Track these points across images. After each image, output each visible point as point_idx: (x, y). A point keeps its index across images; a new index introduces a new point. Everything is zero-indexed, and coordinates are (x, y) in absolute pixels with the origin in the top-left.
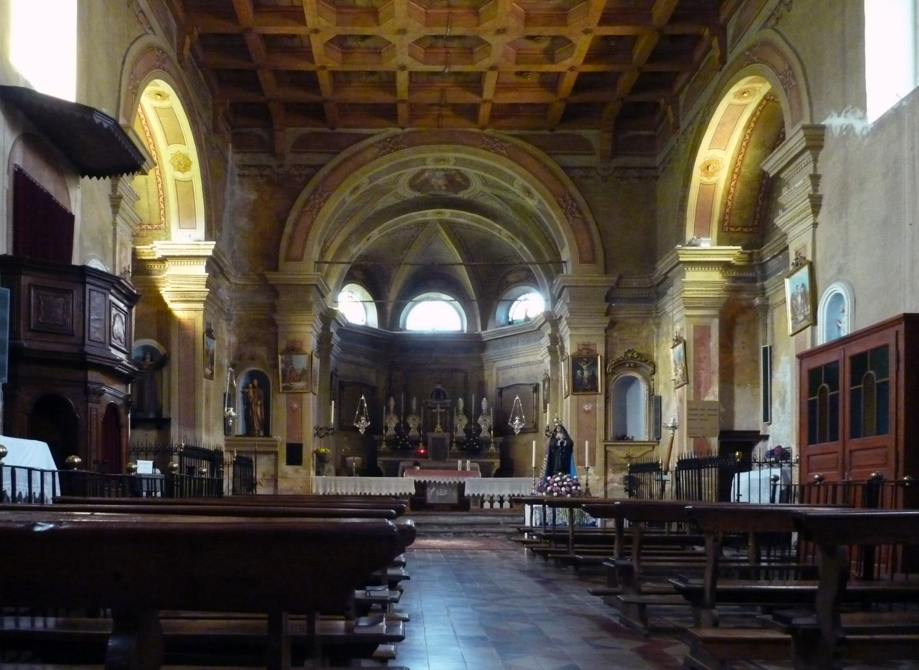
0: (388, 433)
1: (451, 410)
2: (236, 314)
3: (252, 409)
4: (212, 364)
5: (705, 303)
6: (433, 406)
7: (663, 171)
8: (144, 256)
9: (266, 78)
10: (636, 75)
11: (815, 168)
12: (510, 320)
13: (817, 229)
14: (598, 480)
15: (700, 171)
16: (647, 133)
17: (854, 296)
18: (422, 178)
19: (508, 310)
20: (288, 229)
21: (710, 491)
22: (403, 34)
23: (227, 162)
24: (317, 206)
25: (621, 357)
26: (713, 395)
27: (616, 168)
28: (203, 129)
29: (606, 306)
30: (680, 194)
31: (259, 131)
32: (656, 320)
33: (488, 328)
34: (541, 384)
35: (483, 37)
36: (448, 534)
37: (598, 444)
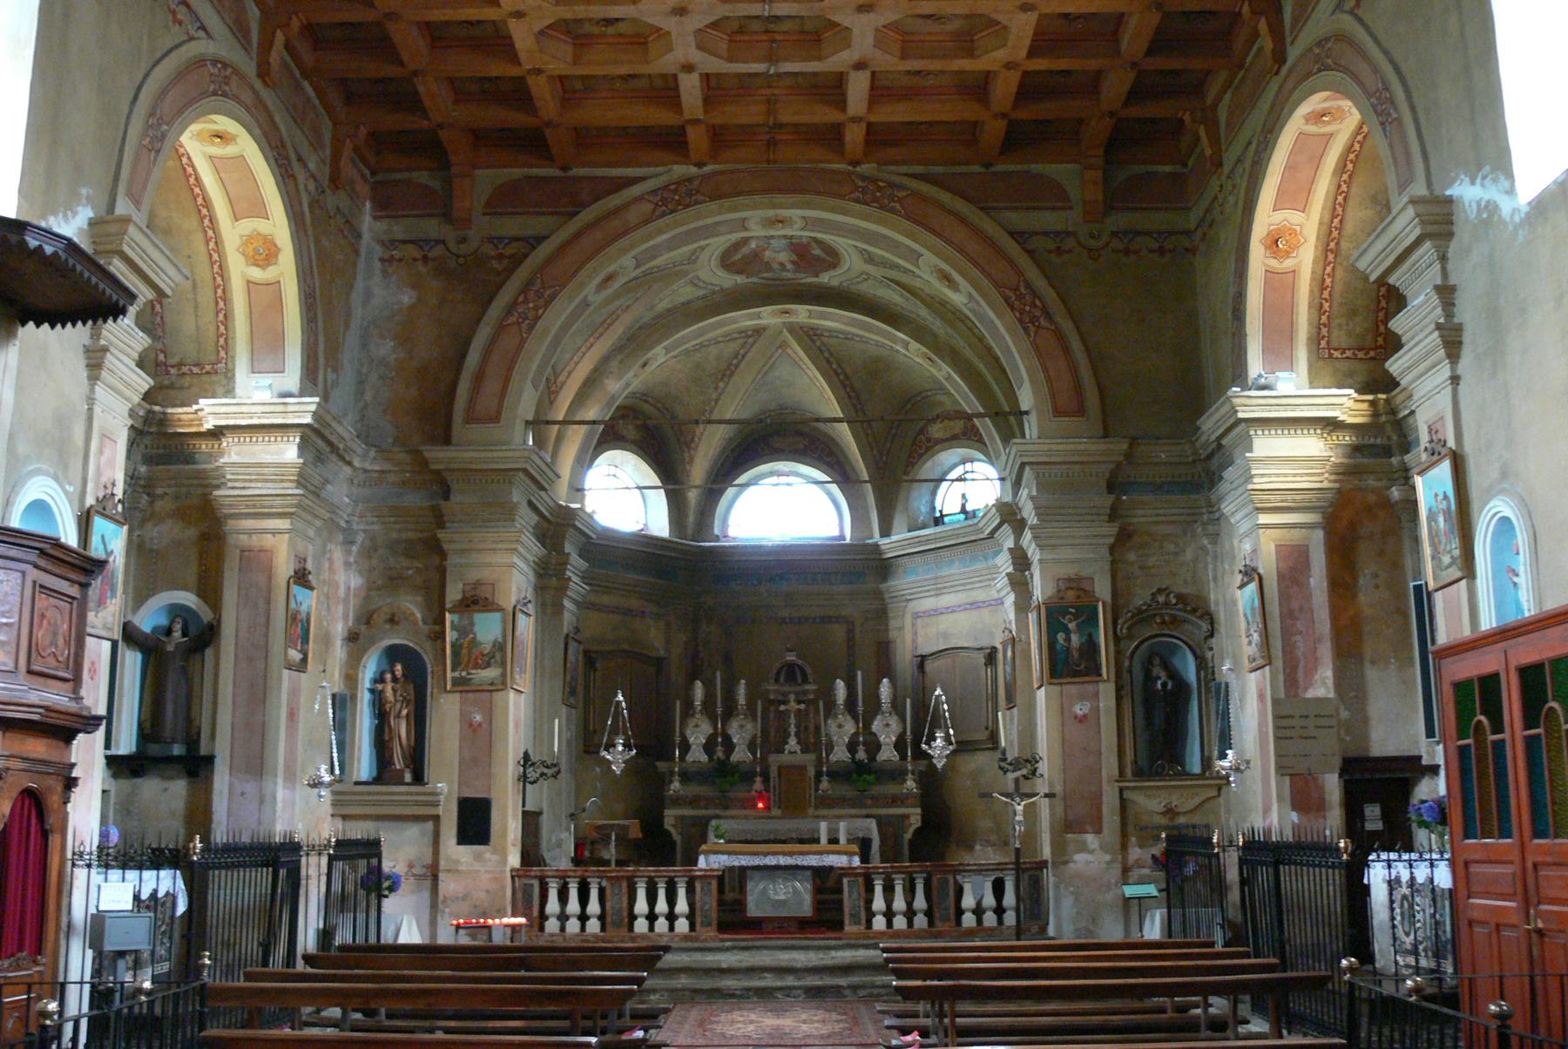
2: (365, 531)
3: (390, 726)
4: (306, 640)
5: (1294, 501)
6: (780, 698)
7: (1203, 239)
8: (182, 426)
9: (433, 92)
10: (1132, 76)
11: (1445, 273)
12: (938, 514)
13: (1460, 387)
14: (1108, 863)
15: (1262, 249)
16: (1167, 169)
17: (1533, 526)
18: (745, 250)
19: (934, 494)
20: (473, 359)
21: (1331, 888)
22: (681, 15)
23: (359, 236)
25: (1144, 604)
26: (1322, 685)
27: (1114, 234)
29: (1108, 500)
30: (1232, 290)
31: (423, 177)
32: (1210, 527)
33: (894, 531)
35: (836, 18)
36: (795, 992)
37: (1105, 787)
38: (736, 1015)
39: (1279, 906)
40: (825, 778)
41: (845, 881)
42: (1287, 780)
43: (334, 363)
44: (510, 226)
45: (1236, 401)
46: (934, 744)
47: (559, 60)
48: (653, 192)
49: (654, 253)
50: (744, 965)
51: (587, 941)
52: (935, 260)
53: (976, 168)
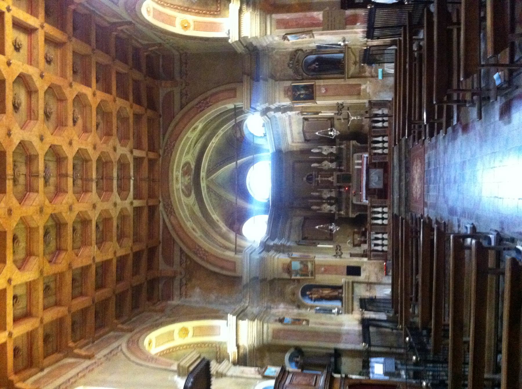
0: (334, 210)
1: (319, 170)
12: (263, 135)
14: (370, 82)
16: (161, 60)
20: (217, 270)
21: (381, 13)
24: (204, 252)
26: (319, 15)
27: (181, 78)
28: (163, 319)
31: (161, 286)
34: (303, 116)
35: (118, 159)
37: (347, 83)
38: (414, 192)
39: (386, 27)
40: (341, 168)
41: (373, 161)
42: (348, 26)
43: (218, 311)
44: (177, 259)
45: (233, 41)
46: (333, 135)
47: (128, 242)
48: (168, 216)
49: (186, 216)
50: (398, 191)
51: (390, 238)
52: (189, 132)
53: (161, 119)
